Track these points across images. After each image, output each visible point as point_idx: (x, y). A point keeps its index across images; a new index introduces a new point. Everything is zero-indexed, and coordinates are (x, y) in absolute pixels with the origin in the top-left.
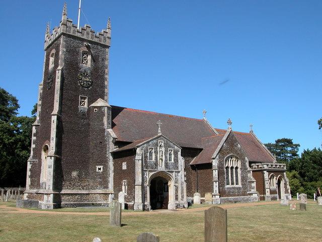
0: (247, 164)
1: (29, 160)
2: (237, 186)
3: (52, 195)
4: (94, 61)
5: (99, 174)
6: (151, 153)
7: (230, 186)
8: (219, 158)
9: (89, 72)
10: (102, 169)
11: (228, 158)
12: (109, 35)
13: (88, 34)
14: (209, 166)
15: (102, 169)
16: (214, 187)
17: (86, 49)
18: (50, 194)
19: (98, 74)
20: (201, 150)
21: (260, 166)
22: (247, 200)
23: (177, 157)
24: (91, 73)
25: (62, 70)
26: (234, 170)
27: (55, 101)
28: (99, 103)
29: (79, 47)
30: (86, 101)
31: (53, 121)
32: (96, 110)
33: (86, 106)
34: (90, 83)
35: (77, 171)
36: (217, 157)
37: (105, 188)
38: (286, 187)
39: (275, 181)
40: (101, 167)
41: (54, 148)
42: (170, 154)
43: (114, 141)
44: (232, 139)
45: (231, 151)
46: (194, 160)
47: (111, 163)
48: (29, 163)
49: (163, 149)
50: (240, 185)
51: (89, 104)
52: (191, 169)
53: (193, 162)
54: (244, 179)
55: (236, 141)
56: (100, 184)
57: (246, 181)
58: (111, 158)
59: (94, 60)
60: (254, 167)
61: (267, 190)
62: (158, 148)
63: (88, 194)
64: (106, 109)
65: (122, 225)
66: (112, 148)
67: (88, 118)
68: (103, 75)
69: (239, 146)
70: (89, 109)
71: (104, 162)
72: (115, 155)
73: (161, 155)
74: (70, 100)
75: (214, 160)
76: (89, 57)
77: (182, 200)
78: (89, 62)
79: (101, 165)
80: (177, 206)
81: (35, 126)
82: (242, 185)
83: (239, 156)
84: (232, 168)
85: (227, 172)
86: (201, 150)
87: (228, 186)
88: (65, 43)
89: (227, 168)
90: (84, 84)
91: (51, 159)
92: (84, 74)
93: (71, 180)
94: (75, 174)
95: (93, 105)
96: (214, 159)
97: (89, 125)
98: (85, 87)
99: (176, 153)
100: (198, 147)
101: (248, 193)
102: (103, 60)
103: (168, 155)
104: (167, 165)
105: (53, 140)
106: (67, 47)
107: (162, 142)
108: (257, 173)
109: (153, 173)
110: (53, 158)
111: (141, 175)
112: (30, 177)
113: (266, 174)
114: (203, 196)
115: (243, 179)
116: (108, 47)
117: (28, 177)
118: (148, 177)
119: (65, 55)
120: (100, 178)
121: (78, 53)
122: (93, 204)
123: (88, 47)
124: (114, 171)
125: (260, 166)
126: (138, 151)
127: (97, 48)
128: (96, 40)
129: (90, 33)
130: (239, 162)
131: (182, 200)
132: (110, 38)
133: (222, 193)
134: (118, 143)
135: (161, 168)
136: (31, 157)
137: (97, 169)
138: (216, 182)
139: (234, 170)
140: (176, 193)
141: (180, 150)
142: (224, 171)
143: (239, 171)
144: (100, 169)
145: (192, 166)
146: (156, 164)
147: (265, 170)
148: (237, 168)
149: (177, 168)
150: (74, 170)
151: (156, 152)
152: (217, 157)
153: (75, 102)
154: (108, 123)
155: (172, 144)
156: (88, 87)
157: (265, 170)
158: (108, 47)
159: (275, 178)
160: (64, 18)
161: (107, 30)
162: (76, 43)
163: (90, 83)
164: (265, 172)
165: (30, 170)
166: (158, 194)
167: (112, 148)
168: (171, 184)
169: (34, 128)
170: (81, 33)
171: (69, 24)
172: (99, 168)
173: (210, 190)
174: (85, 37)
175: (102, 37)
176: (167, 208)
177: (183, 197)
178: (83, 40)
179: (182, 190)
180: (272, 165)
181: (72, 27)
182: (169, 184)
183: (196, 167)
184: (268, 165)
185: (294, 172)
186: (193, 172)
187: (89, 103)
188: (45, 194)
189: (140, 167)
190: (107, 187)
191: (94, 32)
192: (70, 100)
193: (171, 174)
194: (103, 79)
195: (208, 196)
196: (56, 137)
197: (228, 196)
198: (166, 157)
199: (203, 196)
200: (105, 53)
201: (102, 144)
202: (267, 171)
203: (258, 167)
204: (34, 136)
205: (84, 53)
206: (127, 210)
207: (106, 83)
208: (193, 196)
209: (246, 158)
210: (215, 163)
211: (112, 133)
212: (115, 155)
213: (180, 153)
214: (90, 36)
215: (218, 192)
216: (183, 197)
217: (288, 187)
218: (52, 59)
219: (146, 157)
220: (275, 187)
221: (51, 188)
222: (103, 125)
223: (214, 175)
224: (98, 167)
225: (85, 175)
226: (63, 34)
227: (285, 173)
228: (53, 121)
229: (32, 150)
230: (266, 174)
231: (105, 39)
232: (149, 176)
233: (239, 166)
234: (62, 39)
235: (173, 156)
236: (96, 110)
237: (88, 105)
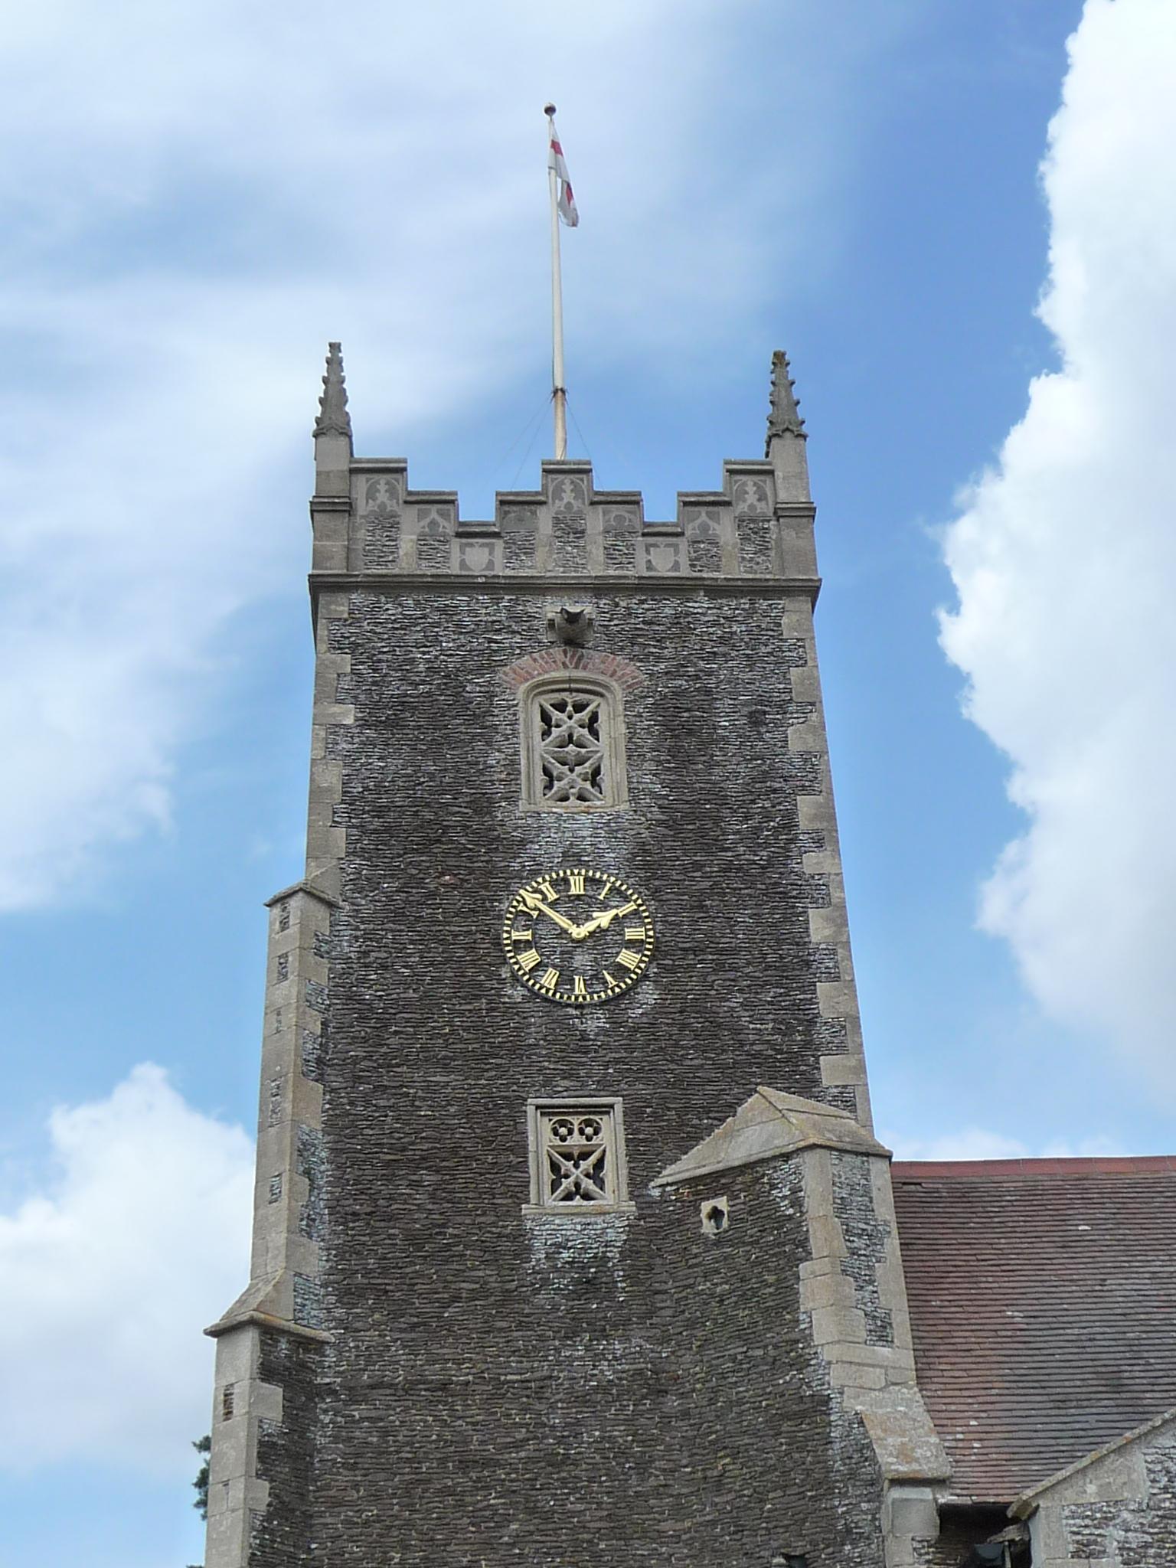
13: (571, 530)
30: (611, 1135)
32: (716, 1214)
33: (614, 1194)
51: (644, 1157)
68: (782, 858)
70: (658, 1228)
78: (614, 773)
102: (756, 720)
119: (349, 760)
174: (542, 564)
192: (423, 1161)
207: (818, 929)
236: (716, 1214)
237: (636, 1185)
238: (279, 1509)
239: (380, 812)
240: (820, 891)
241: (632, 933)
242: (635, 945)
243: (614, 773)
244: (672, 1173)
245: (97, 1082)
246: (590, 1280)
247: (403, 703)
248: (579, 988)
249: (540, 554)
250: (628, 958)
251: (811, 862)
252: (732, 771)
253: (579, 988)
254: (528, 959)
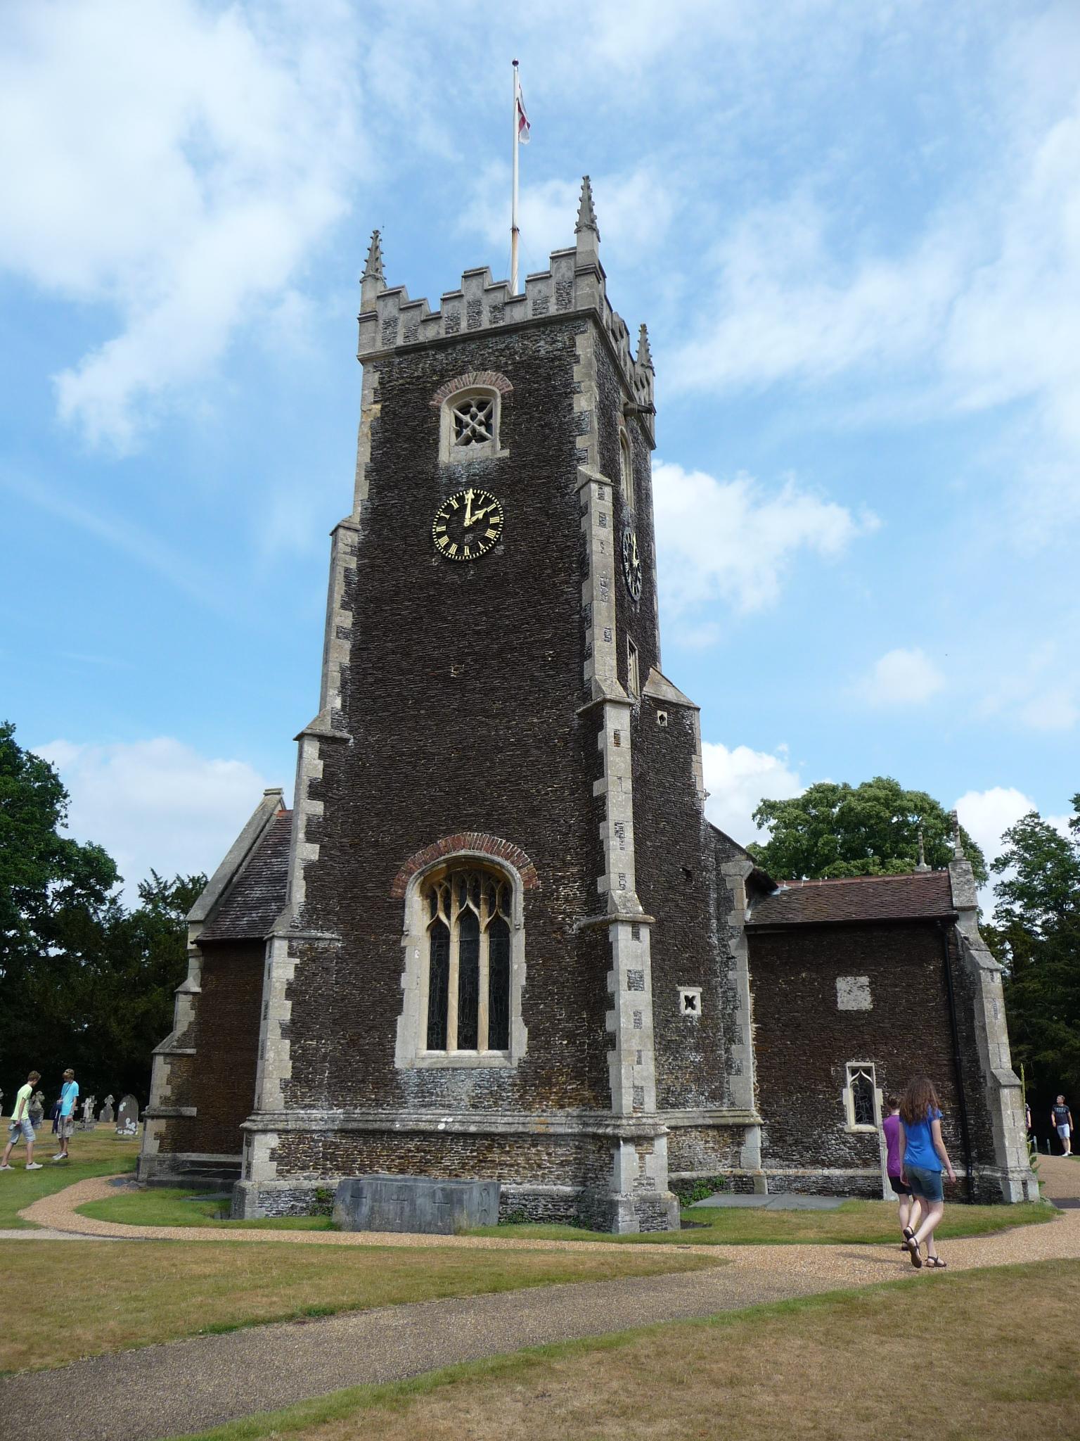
31: (617, 736)
91: (636, 935)
120: (697, 1048)
188: (627, 1140)
224: (685, 992)
228: (617, 736)
241: (493, 520)
242: (495, 527)
248: (467, 551)
250: (491, 534)
253: (467, 551)
254: (444, 541)
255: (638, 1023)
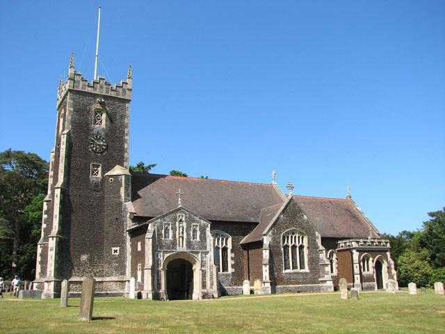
0: (319, 241)
1: (40, 242)
2: (302, 271)
3: (53, 283)
4: (112, 122)
5: (115, 258)
6: (167, 230)
7: (291, 271)
8: (273, 233)
9: (103, 133)
10: (118, 251)
11: (288, 233)
12: (129, 86)
13: (102, 87)
14: (259, 244)
15: (118, 251)
16: (264, 272)
17: (99, 106)
18: (51, 282)
19: (116, 135)
20: (258, 223)
21: (348, 244)
22: (319, 290)
23: (205, 234)
24: (106, 135)
25: (68, 134)
26: (298, 249)
27: (60, 171)
28: (117, 170)
29: (91, 104)
30: (100, 169)
33: (99, 175)
34: (104, 147)
35: (87, 254)
36: (270, 233)
37: (121, 274)
38: (389, 272)
39: (371, 264)
40: (118, 249)
41: (57, 227)
42: (195, 231)
43: (132, 217)
44: (292, 210)
45: (292, 224)
46: (245, 238)
47: (128, 244)
48: (39, 246)
49: (185, 224)
50: (307, 270)
52: (241, 250)
53: (244, 240)
54: (314, 261)
55: (300, 211)
56: (116, 269)
57: (317, 264)
58: (128, 237)
59: (111, 119)
60: (341, 245)
61: (357, 277)
62: (177, 223)
63: (102, 282)
64: (123, 177)
65: (93, 319)
66: (130, 225)
67: (102, 189)
68: (122, 137)
69: (305, 217)
70: (104, 179)
71: (121, 243)
72: (133, 233)
73: (181, 231)
74: (78, 169)
75: (265, 237)
76: (104, 116)
77: (211, 288)
78: (104, 122)
79: (117, 246)
80: (205, 296)
81: (47, 201)
82: (310, 269)
83: (308, 231)
84: (294, 247)
85: (286, 253)
86: (258, 223)
87: (287, 271)
88: (72, 102)
89: (286, 247)
90: (96, 149)
92: (97, 137)
93: (80, 264)
94: (84, 257)
95: (109, 173)
96: (264, 235)
97: (103, 198)
98: (98, 153)
99: (203, 230)
100: (253, 220)
101: (320, 279)
102: (121, 117)
103: (191, 232)
104: (189, 244)
105: (56, 217)
106: (74, 106)
107: (183, 216)
108: (345, 253)
109: (169, 254)
110: (55, 239)
111: (151, 256)
112: (40, 263)
113: (356, 255)
114: (252, 284)
115: (312, 261)
116: (128, 101)
117: (38, 263)
118: (162, 259)
119: (72, 116)
120: (116, 262)
121: (89, 112)
122: (107, 294)
123: (101, 103)
124: (132, 254)
125: (348, 244)
126: (149, 228)
127: (115, 105)
128: (113, 94)
129: (105, 86)
130: (306, 239)
131: (211, 288)
132: (131, 90)
133: (274, 282)
134: (136, 219)
135: (182, 248)
136: (42, 238)
137: (113, 251)
138: (265, 265)
139: (298, 249)
140: (202, 279)
141: (209, 225)
142: (280, 250)
143: (306, 251)
144: (116, 251)
145: (242, 245)
146: (174, 243)
147: (354, 249)
148: (301, 247)
149: (206, 248)
150: (84, 253)
151: (174, 229)
152: (270, 233)
153: (85, 171)
154: (126, 195)
155: (197, 219)
156: (101, 153)
157: (354, 249)
158: (128, 101)
159: (371, 259)
160: (71, 71)
161: (128, 81)
162: (86, 100)
163: (104, 147)
164: (354, 251)
165: (41, 255)
166: (178, 281)
167: (130, 225)
168: (197, 268)
169: (45, 204)
170: (116, 91)
171: (77, 78)
172: (115, 251)
173: (260, 276)
174: (97, 92)
175: (121, 90)
176: (191, 298)
177: (212, 284)
178: (95, 96)
179: (211, 275)
180: (365, 242)
181: (81, 82)
182: (193, 268)
183: (247, 247)
184: (358, 242)
185: (425, 252)
186: (245, 253)
187: (104, 171)
189: (151, 247)
190: (124, 274)
191: (86, 81)
192: (78, 169)
193: (196, 256)
194: (122, 141)
195: (257, 283)
196: (60, 214)
197: (287, 284)
198: (188, 234)
199: (252, 284)
200: (124, 109)
201: (119, 221)
202: (357, 251)
203: (346, 245)
204: (45, 214)
205: (97, 111)
206: (158, 302)
207: (126, 146)
208: (242, 284)
209: (317, 233)
210: (267, 241)
211: (130, 207)
212: (133, 233)
213: (208, 229)
214: (104, 90)
215: (268, 278)
216: (212, 284)
217: (394, 272)
218: (62, 120)
219: (160, 235)
220: (371, 271)
221: (53, 274)
222: (120, 197)
223: (264, 257)
224: (113, 249)
225: (99, 258)
226: (69, 90)
227: (388, 254)
229: (42, 230)
230: (356, 255)
231: (124, 91)
232: (163, 257)
233: (305, 244)
234: (68, 97)
235: (198, 233)
237: (102, 175)
238: (57, 286)
239: (75, 123)
240: (126, 141)
243: (104, 122)
244: (106, 174)
245: (397, 237)
246: (96, 185)
247: (79, 109)
249: (98, 90)
251: (126, 137)
252: (118, 124)
255: (51, 258)
